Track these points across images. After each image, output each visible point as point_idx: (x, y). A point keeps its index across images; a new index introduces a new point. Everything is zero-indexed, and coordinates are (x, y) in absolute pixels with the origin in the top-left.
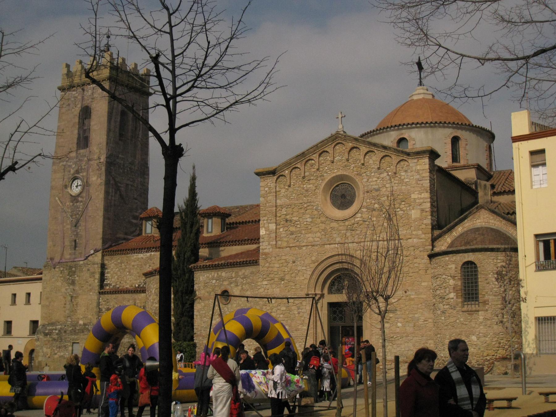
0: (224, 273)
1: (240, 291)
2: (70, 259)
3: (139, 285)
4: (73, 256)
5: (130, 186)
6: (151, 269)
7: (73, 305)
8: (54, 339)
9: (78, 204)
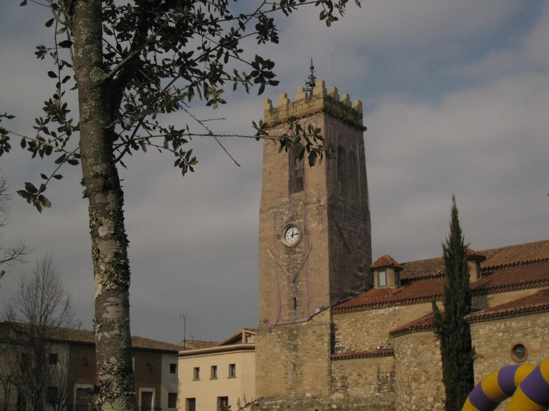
0: (514, 323)
1: (541, 344)
2: (289, 320)
3: (381, 347)
4: (294, 317)
5: (353, 233)
6: (396, 327)
9: (295, 256)
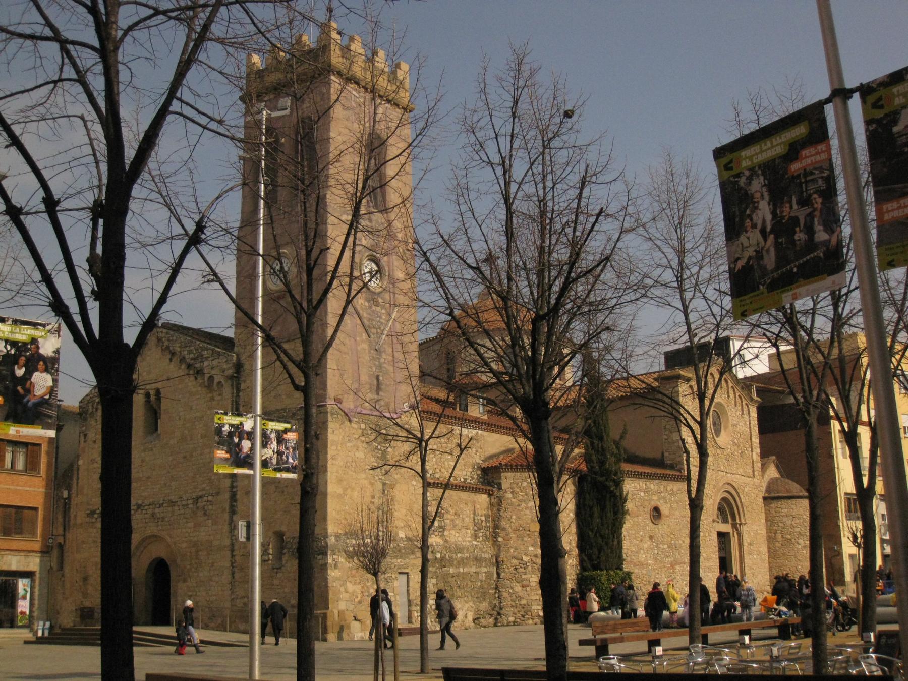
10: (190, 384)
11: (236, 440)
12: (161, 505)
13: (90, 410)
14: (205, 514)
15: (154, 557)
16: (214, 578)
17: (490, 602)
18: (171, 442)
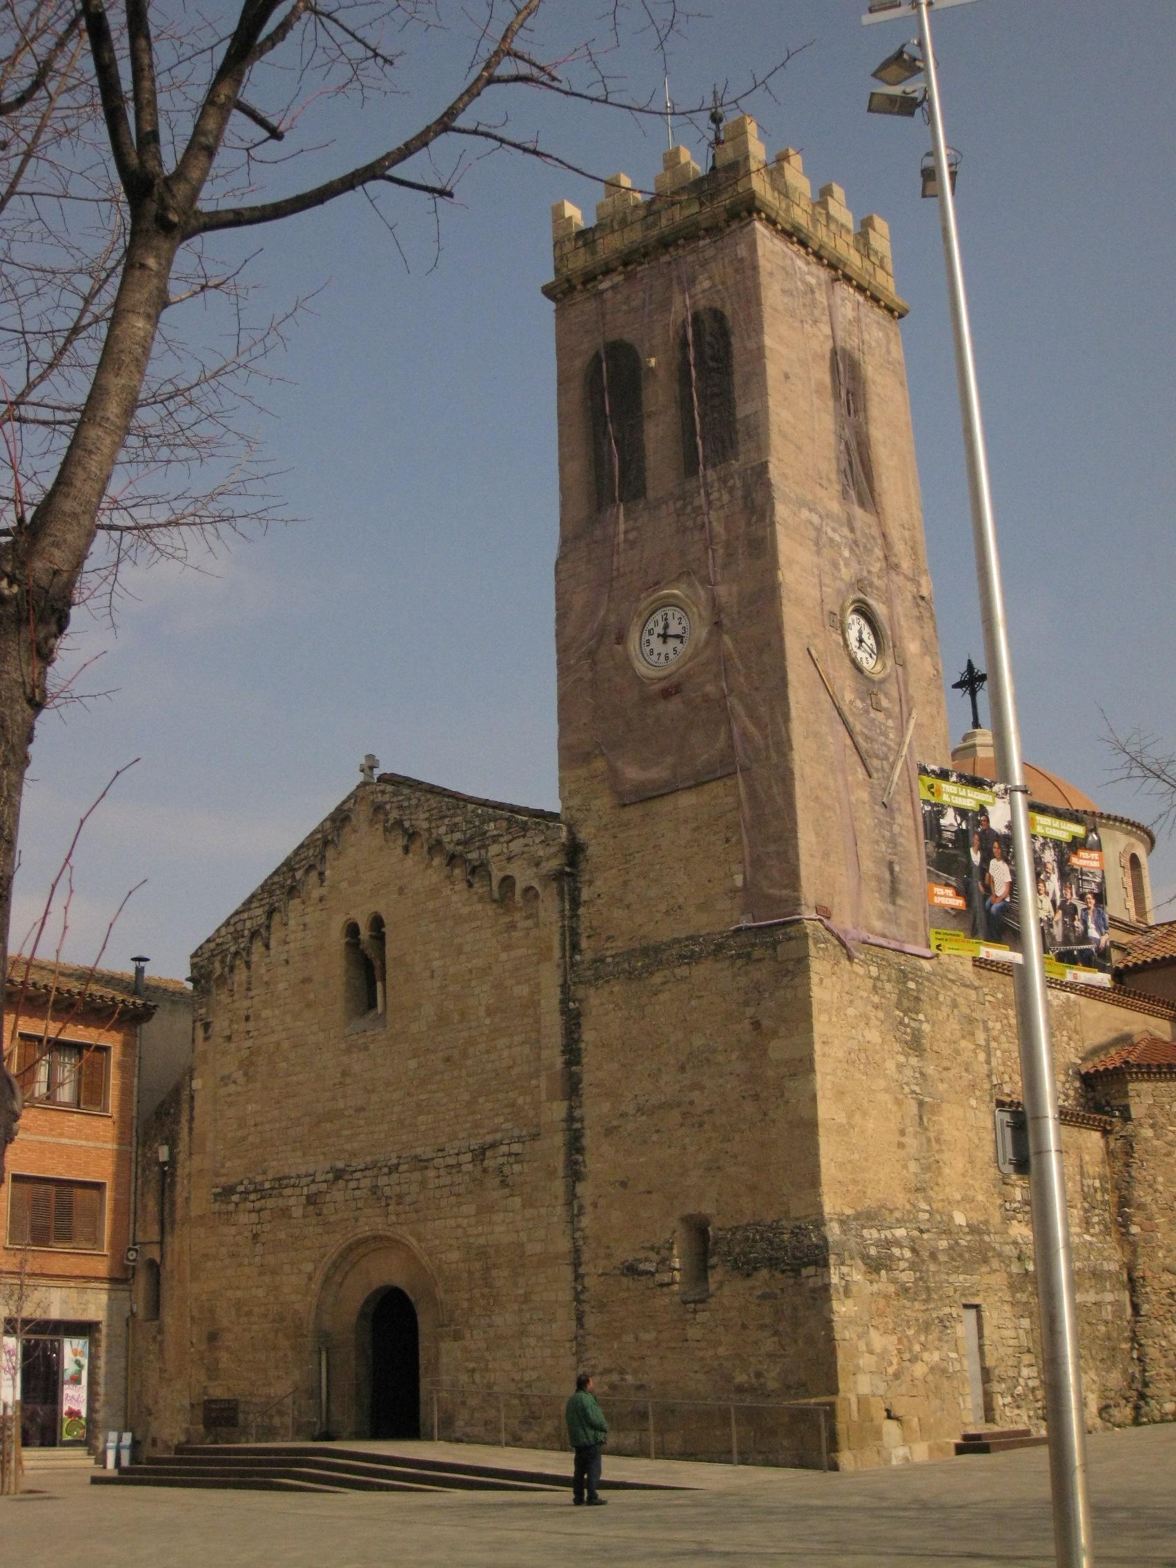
7: (929, 1140)
8: (904, 1290)
10: (455, 898)
11: (976, 857)
12: (394, 1169)
13: (218, 972)
14: (504, 1184)
15: (376, 1283)
16: (531, 1328)
17: (1125, 1371)
18: (414, 1028)
